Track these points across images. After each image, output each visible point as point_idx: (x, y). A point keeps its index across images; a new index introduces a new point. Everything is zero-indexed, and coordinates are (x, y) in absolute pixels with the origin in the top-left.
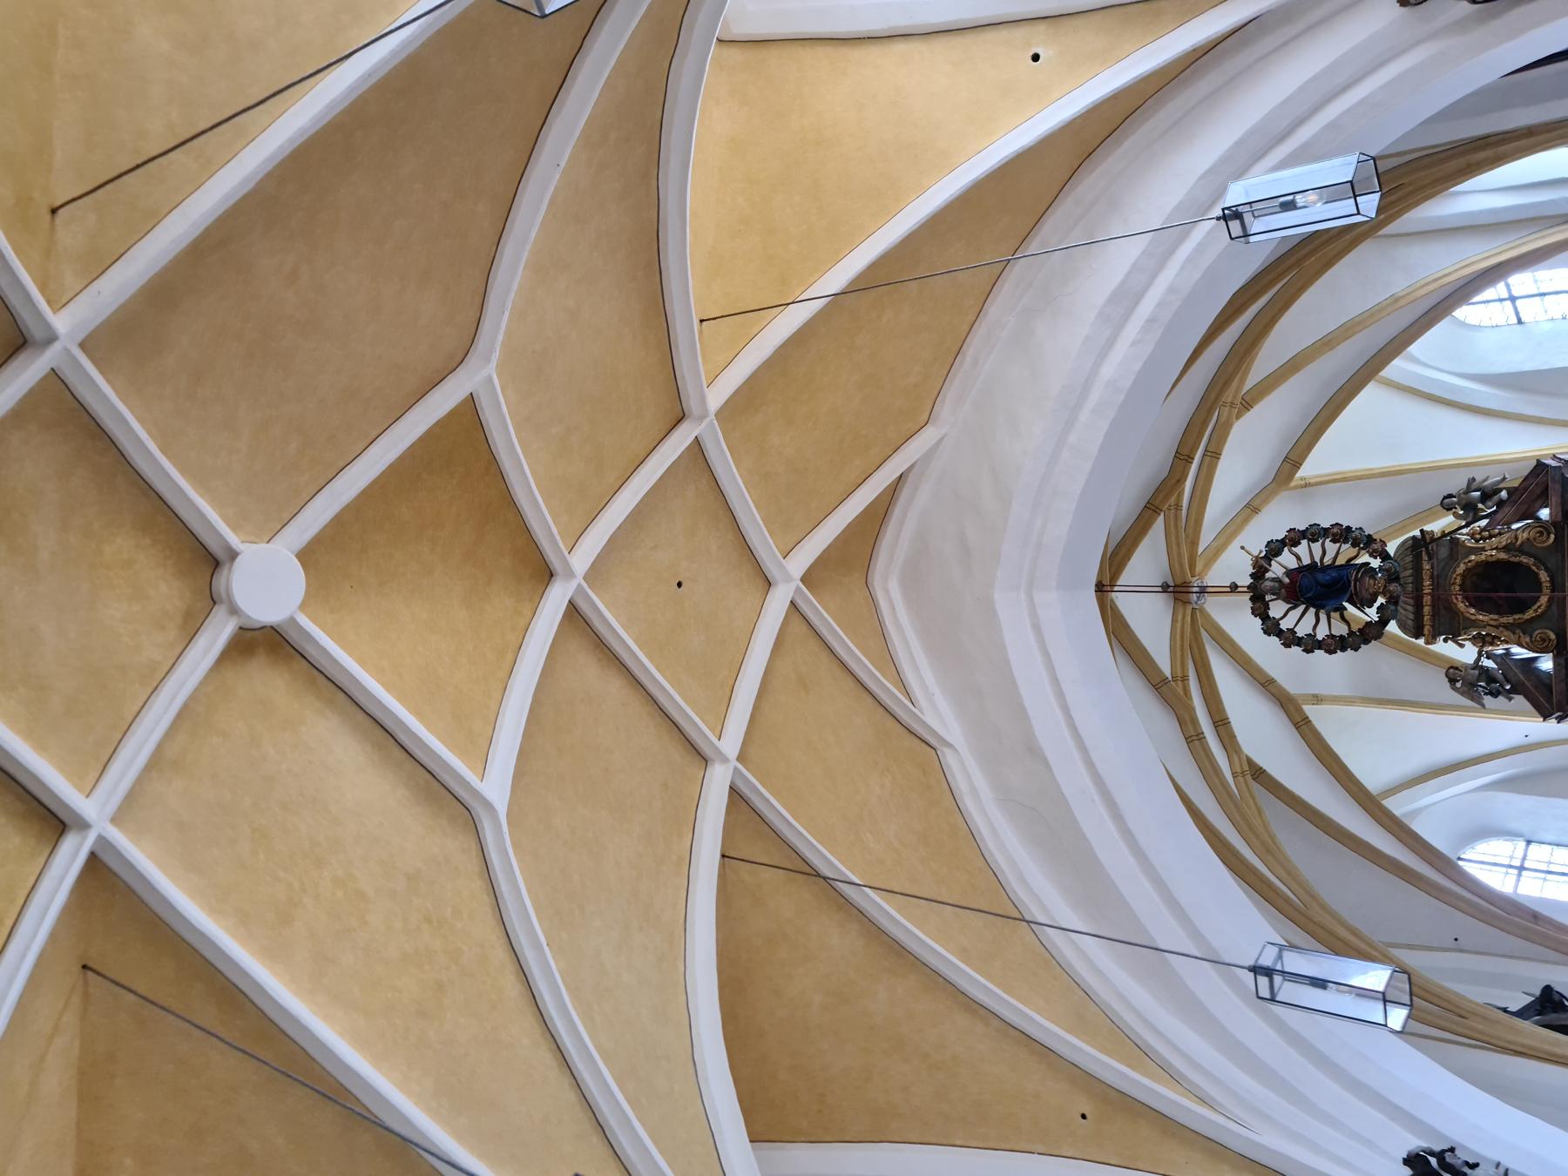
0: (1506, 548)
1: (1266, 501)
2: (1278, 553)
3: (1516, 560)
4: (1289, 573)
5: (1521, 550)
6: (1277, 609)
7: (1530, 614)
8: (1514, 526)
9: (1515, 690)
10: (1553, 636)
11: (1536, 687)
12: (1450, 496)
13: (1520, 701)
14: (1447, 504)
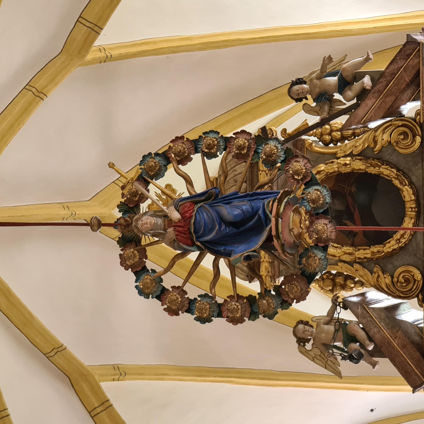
0: (364, 155)
1: (53, 81)
2: (159, 174)
3: (372, 170)
4: (180, 204)
5: (380, 159)
6: (159, 254)
7: (391, 245)
8: (372, 125)
9: (379, 352)
10: (418, 276)
11: (403, 347)
12: (300, 81)
13: (385, 364)
14: (295, 91)
